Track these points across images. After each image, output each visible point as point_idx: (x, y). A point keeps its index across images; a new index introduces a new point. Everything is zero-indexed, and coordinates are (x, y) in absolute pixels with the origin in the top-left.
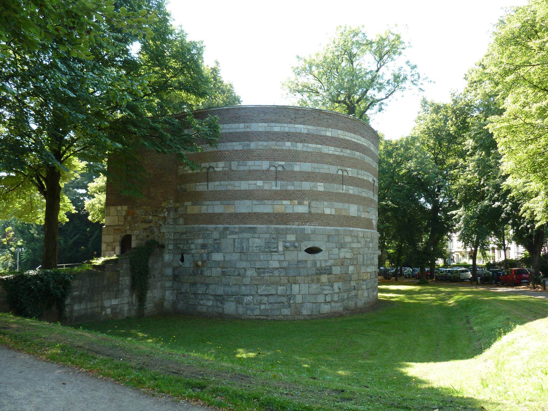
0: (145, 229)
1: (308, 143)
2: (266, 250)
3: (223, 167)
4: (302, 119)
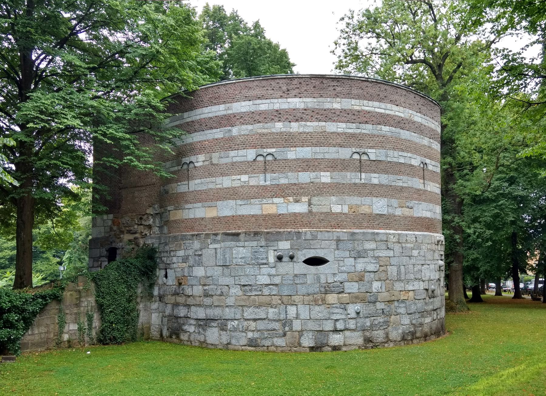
0: (130, 241)
1: (307, 121)
2: (254, 262)
3: (203, 161)
4: (297, 90)
